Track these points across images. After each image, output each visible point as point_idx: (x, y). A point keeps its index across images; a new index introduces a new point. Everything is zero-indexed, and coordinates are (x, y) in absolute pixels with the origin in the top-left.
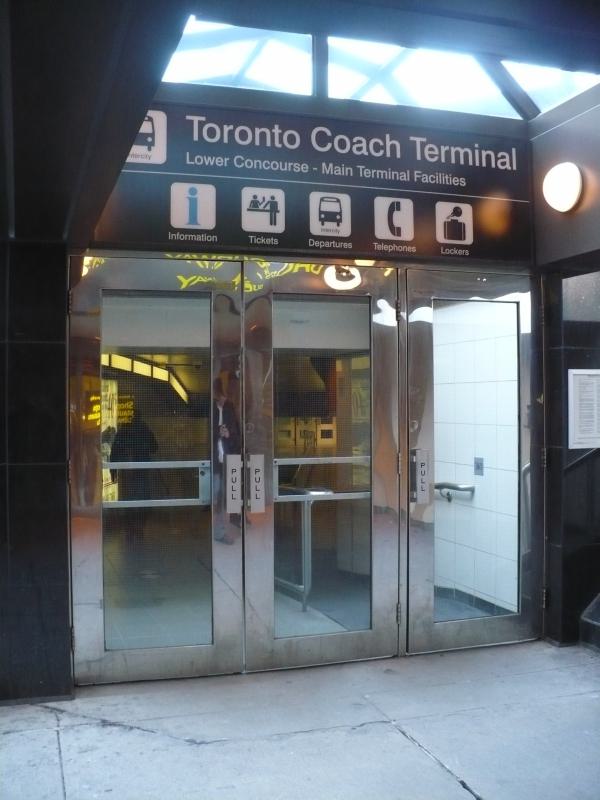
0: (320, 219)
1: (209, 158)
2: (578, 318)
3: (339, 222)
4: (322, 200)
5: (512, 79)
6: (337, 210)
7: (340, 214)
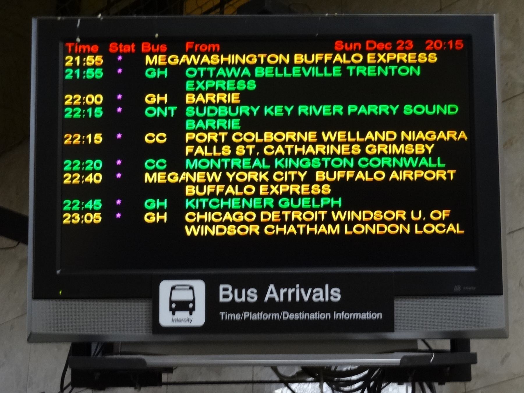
0: (171, 309)
1: (330, 133)
2: (187, 311)
3: (191, 311)
4: (173, 288)
5: (35, 133)
6: (191, 298)
7: (193, 302)
